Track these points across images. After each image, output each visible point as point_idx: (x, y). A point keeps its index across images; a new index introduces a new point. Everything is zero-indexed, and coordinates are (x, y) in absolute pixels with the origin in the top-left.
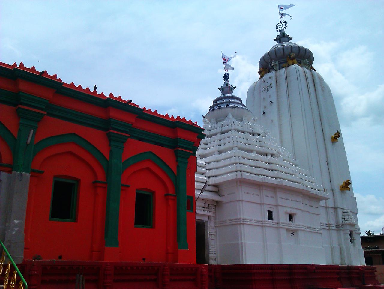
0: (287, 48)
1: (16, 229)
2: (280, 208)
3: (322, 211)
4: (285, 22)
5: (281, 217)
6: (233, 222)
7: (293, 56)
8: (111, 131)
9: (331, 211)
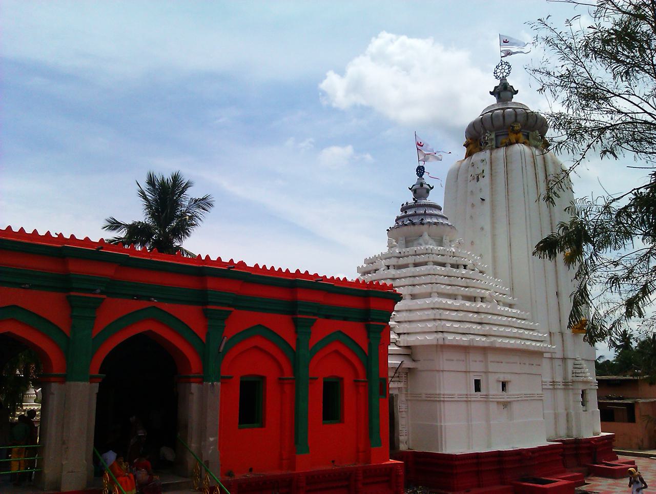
0: (510, 114)
1: (212, 448)
2: (490, 375)
3: (546, 364)
5: (492, 388)
7: (518, 128)
9: (559, 362)
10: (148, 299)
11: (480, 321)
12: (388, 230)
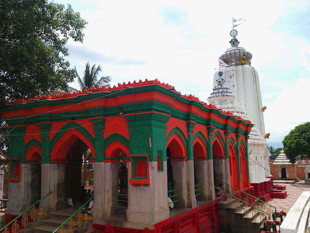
8: (154, 112)
12: (209, 97)
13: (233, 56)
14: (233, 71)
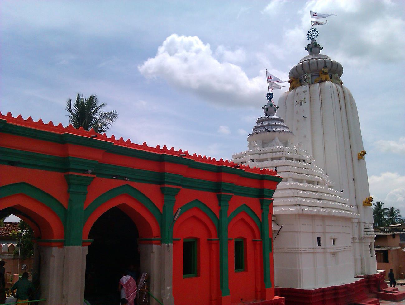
0: (321, 62)
1: (169, 294)
4: (316, 30)
5: (327, 243)
6: (291, 250)
9: (356, 225)
10: (123, 178)
11: (319, 198)
13: (307, 69)
14: (304, 94)
